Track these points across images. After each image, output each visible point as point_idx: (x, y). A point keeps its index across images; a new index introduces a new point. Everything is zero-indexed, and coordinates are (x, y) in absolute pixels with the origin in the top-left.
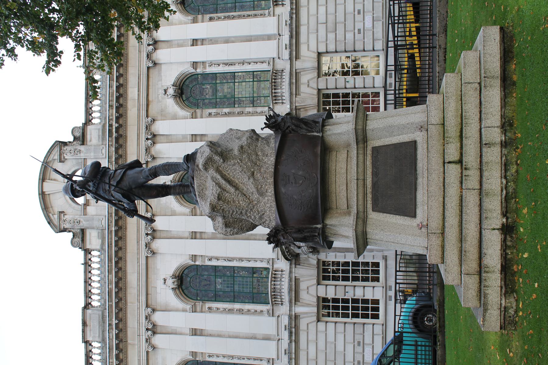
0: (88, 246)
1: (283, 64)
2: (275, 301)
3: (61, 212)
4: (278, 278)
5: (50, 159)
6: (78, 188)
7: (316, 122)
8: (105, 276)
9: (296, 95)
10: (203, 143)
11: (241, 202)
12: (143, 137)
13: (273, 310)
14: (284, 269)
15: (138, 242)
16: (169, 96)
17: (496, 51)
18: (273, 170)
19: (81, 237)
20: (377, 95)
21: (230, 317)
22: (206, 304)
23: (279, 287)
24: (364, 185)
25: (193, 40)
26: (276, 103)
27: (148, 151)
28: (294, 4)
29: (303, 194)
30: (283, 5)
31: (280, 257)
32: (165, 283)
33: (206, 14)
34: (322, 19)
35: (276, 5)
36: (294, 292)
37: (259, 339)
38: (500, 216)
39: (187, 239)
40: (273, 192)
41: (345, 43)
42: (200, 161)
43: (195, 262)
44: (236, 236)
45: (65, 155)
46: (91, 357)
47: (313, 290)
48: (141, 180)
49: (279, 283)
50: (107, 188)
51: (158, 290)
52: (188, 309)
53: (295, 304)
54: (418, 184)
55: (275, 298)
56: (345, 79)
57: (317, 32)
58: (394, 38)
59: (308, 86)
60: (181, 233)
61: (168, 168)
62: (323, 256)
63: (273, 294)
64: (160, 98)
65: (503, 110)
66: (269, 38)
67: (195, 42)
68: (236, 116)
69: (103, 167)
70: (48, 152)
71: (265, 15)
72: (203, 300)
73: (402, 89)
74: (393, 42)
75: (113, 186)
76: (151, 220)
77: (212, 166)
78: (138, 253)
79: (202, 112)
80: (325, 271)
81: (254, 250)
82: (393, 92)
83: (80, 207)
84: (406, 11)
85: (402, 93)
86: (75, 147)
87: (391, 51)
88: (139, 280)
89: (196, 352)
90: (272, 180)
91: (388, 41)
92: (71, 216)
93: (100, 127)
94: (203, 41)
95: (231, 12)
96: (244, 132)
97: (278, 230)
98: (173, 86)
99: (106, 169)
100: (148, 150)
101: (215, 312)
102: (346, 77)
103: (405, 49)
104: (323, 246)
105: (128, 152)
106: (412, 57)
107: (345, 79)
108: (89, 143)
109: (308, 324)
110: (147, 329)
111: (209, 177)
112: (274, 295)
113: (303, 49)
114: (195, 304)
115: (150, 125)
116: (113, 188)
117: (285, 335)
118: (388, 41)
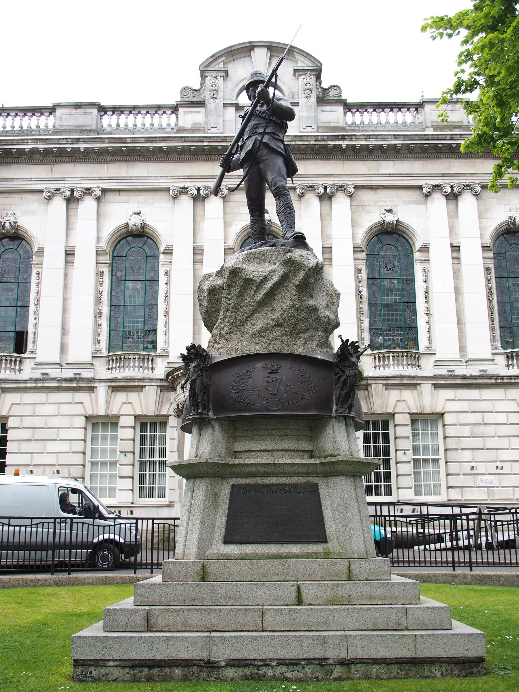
0: (181, 110)
1: (428, 368)
2: (113, 360)
3: (226, 72)
4: (144, 364)
5: (298, 57)
6: (259, 89)
7: (350, 409)
8: (142, 133)
9: (386, 385)
10: (320, 258)
11: (242, 310)
12: (328, 182)
13: (101, 357)
14: (155, 371)
15: (189, 177)
16: (383, 216)
17: (451, 652)
18: (285, 352)
19: (195, 99)
20: (388, 491)
21: (91, 300)
22: (107, 269)
23: (132, 364)
24: (267, 475)
25: (460, 247)
26: (375, 358)
27: (310, 189)
28: (509, 381)
29: (253, 392)
30: (508, 366)
31: (170, 365)
32: (135, 214)
33: (494, 263)
34: (490, 418)
35: (508, 357)
36: (124, 384)
37: (62, 338)
38: (226, 657)
39: (194, 243)
40: (256, 352)
41: (457, 449)
42: (297, 253)
43: (163, 253)
44: (197, 304)
45: (303, 77)
46: (33, 114)
47: (127, 409)
48: (270, 177)
49: (137, 364)
50: (260, 130)
51: (125, 205)
52: (100, 245)
53: (109, 386)
54: (269, 546)
55: (117, 359)
56: (409, 450)
57: (472, 412)
58: (464, 515)
59: (398, 401)
60: (201, 234)
61: (287, 213)
62: (174, 422)
63: (122, 357)
64: (381, 204)
65: (370, 661)
66: (462, 348)
67: (455, 248)
68: (357, 306)
69: (287, 125)
70: (308, 54)
71: (494, 342)
72: (112, 265)
73: (396, 526)
74: (459, 513)
75: (262, 139)
76: (217, 191)
77: (290, 271)
78: (173, 178)
79: (363, 260)
80: (153, 425)
81: (180, 329)
82: (392, 513)
83: (234, 98)
84: (503, 531)
85: (390, 526)
86: (315, 89)
87: (448, 511)
88: (138, 178)
89: (43, 255)
90: (272, 350)
91: (461, 506)
92: (222, 86)
93: (341, 124)
94: (456, 260)
95: (497, 296)
96: (335, 312)
97: (205, 360)
98: (397, 221)
99: (285, 128)
100: (311, 188)
101: (97, 280)
102: (411, 450)
103: (451, 530)
104: (184, 420)
105: (307, 162)
106: (439, 538)
107: (409, 450)
108: (320, 108)
109: (82, 403)
110: (72, 191)
111: (274, 267)
112: (121, 359)
113: (449, 393)
114: (107, 253)
115: (344, 191)
116: (259, 138)
117: (68, 374)
118: (461, 506)
